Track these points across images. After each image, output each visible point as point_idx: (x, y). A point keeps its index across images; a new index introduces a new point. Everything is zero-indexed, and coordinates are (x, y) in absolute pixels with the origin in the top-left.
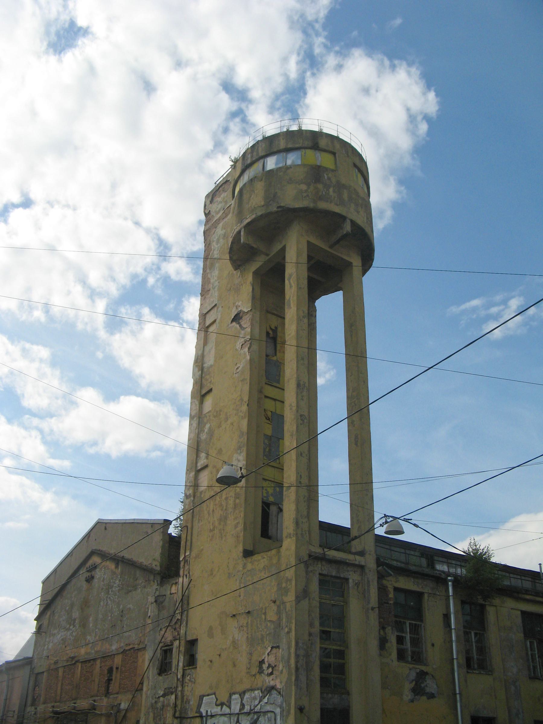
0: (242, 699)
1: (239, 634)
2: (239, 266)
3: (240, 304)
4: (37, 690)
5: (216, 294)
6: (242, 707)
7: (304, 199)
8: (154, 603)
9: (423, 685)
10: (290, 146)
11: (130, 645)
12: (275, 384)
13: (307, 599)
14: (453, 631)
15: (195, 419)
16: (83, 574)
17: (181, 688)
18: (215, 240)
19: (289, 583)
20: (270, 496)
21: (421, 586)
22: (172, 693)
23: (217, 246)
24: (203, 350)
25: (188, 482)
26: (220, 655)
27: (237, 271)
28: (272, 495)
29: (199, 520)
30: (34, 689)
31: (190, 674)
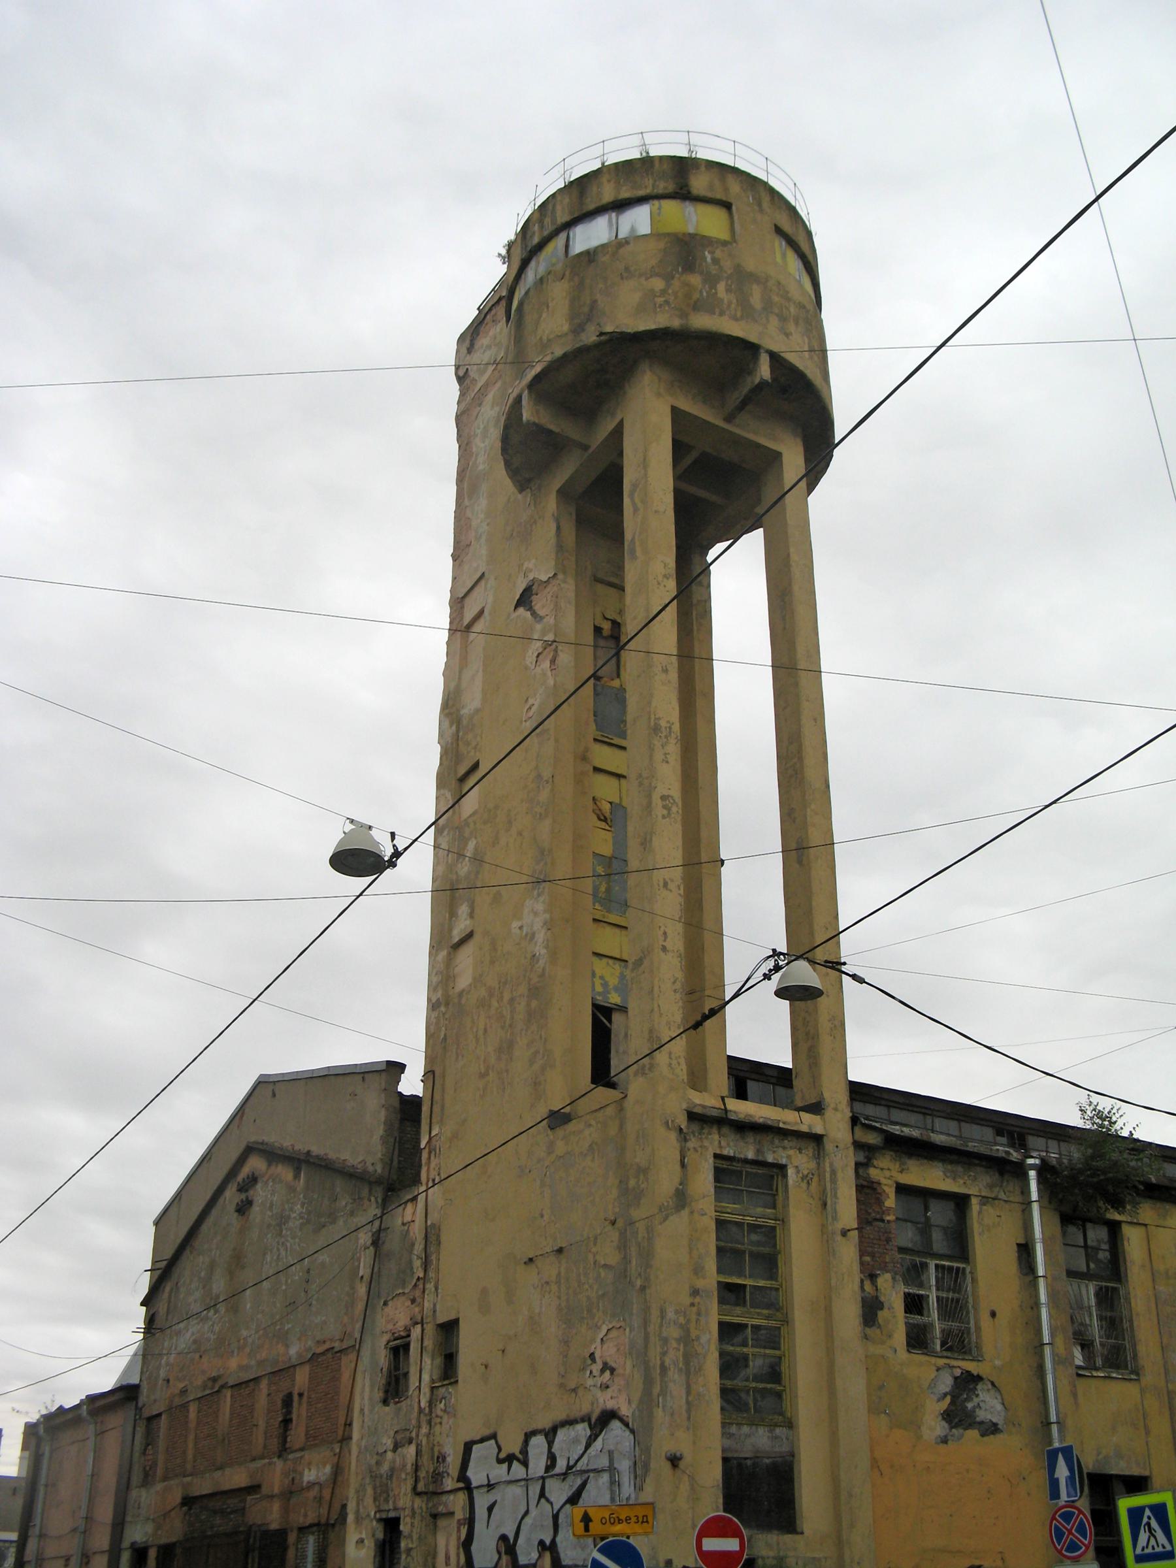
0: (550, 1444)
1: (541, 1300)
2: (529, 480)
3: (531, 566)
4: (151, 1452)
5: (484, 552)
6: (551, 1462)
7: (658, 310)
8: (371, 1248)
9: (970, 1405)
10: (625, 194)
11: (324, 1342)
12: (616, 741)
13: (685, 1213)
14: (1041, 1282)
15: (446, 833)
16: (231, 1195)
17: (428, 1427)
18: (478, 431)
19: (642, 1177)
20: (612, 992)
21: (962, 1182)
22: (410, 1442)
23: (482, 445)
24: (460, 678)
25: (434, 974)
26: (503, 1351)
27: (524, 493)
28: (616, 989)
29: (457, 1055)
30: (145, 1449)
31: (445, 1398)
